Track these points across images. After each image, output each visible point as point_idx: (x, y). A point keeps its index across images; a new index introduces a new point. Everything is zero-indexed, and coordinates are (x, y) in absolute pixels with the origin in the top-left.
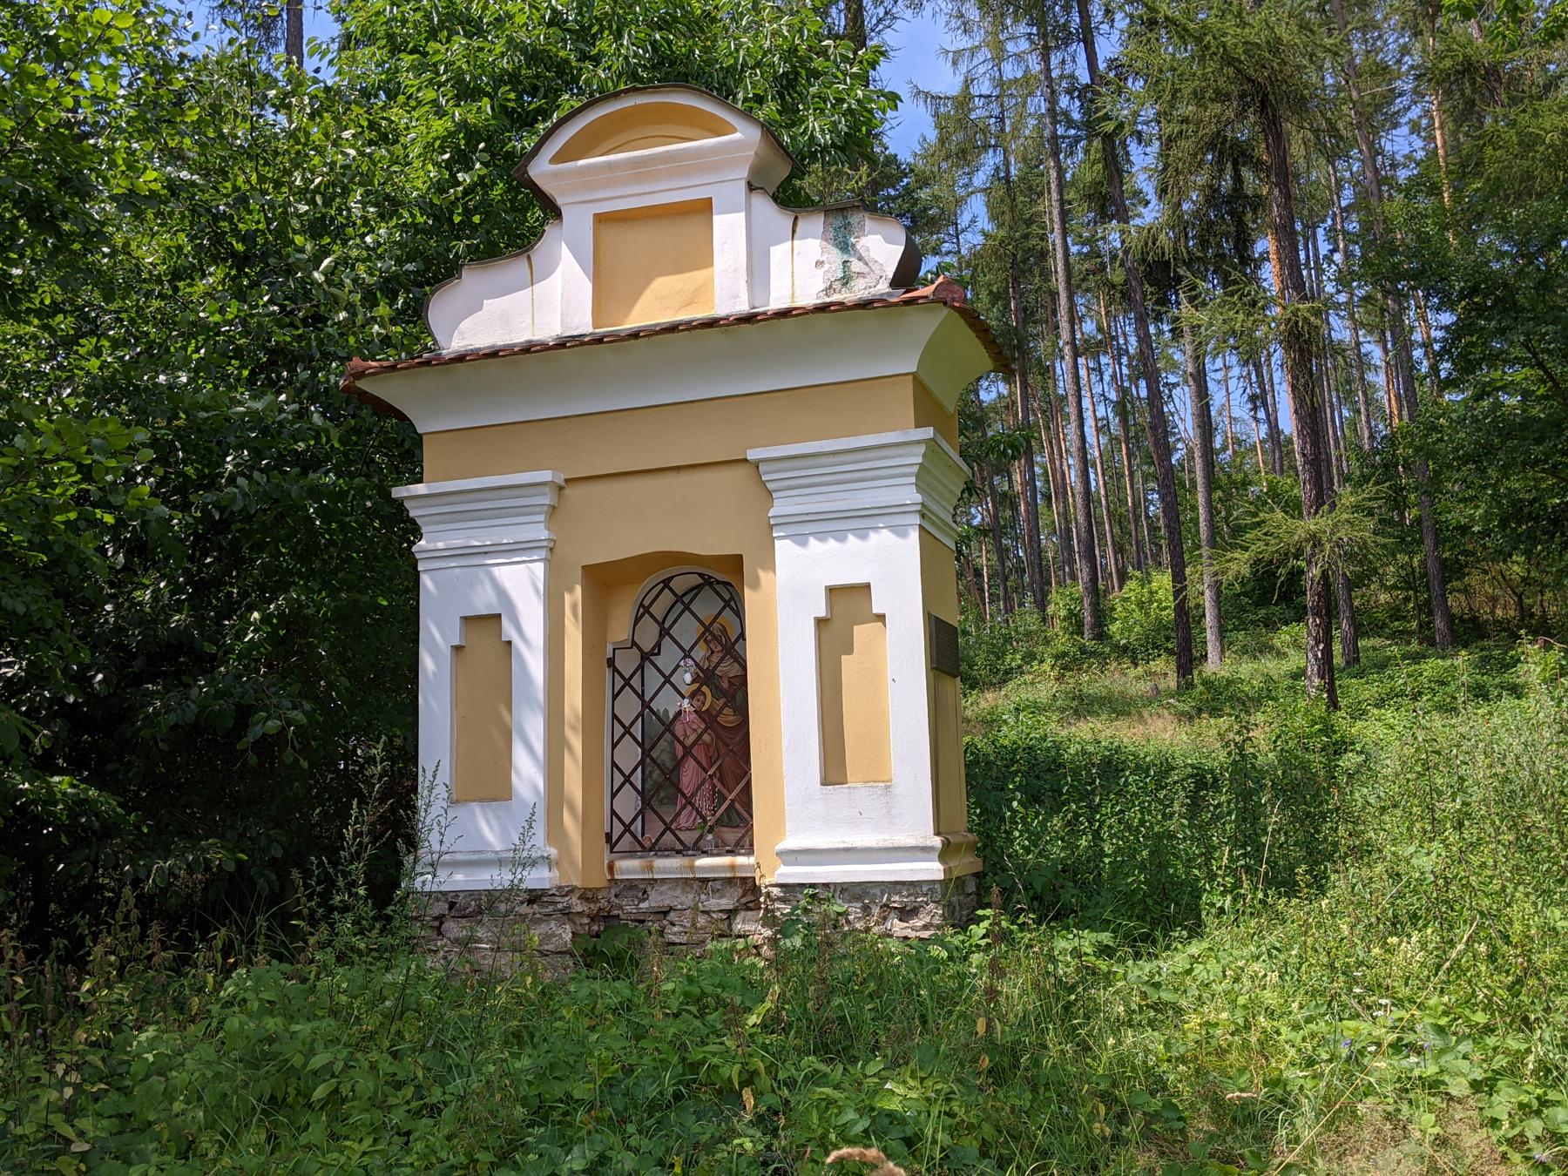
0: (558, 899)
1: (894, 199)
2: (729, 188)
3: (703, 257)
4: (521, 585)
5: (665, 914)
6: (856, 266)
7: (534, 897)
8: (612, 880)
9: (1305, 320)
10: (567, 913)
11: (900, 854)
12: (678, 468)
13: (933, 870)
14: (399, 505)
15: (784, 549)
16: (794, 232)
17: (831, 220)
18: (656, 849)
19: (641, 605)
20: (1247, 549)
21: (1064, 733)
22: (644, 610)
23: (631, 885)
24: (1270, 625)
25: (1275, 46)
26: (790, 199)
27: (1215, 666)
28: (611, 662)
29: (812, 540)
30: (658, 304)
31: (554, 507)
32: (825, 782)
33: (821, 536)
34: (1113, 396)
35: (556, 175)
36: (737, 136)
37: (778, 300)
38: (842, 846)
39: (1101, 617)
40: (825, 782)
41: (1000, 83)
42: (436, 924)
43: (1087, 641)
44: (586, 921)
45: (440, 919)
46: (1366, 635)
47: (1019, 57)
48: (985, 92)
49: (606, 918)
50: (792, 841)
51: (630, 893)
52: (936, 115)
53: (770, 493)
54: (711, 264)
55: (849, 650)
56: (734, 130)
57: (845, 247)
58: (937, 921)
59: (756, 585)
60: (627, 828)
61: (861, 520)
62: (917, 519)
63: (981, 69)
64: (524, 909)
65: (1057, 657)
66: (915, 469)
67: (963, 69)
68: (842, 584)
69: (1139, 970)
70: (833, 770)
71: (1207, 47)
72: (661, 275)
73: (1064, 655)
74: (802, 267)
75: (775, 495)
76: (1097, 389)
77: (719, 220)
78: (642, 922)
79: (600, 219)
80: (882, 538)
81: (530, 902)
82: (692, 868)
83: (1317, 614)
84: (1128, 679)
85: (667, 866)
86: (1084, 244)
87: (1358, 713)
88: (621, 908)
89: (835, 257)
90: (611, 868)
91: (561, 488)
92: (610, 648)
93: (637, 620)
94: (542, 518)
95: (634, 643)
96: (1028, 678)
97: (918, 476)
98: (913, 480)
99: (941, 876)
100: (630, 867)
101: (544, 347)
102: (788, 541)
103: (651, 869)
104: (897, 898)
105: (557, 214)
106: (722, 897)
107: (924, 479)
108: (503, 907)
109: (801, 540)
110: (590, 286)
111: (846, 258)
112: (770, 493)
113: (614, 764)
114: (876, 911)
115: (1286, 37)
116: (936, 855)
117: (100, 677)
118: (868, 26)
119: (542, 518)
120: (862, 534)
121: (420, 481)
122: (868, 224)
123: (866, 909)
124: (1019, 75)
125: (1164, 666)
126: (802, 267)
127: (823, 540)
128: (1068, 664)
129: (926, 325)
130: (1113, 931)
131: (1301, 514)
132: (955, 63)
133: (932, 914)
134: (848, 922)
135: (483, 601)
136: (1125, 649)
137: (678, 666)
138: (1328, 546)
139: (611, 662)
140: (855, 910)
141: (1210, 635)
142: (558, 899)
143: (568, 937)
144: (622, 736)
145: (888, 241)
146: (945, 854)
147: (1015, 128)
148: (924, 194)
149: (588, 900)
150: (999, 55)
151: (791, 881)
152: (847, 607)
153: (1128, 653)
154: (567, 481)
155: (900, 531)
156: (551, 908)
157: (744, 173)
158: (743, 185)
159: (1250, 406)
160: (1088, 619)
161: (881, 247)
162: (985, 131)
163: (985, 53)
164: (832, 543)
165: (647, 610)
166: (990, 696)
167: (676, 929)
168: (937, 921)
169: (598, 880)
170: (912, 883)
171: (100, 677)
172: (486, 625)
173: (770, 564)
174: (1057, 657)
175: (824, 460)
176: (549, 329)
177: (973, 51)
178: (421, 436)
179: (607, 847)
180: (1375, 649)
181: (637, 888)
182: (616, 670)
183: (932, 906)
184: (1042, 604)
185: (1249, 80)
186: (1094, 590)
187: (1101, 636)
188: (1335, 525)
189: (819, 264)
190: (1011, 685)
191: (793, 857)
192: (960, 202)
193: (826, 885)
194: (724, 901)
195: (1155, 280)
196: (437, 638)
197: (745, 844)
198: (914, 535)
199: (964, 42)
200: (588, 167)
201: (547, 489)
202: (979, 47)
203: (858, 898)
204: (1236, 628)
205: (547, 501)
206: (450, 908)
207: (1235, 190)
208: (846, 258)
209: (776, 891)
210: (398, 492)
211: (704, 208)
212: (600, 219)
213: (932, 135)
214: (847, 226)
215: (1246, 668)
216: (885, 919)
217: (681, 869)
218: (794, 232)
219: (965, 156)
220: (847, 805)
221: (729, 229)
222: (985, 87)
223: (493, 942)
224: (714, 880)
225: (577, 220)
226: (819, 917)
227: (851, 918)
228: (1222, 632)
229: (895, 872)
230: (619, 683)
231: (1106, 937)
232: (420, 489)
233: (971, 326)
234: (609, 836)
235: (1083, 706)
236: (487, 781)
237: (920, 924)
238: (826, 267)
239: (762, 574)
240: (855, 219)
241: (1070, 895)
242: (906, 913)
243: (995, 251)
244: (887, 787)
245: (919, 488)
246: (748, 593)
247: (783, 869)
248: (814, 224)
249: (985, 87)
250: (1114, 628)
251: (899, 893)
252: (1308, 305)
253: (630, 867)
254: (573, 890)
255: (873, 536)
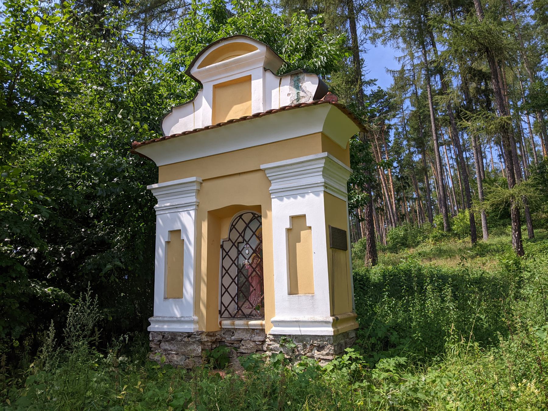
0: (197, 336)
1: (383, 102)
2: (257, 71)
3: (248, 97)
4: (187, 220)
5: (241, 341)
6: (302, 94)
7: (189, 335)
8: (221, 328)
9: (505, 122)
10: (201, 342)
11: (317, 324)
12: (239, 174)
13: (329, 331)
14: (149, 191)
15: (275, 202)
16: (280, 84)
17: (293, 78)
18: (233, 317)
19: (232, 225)
20: (488, 200)
21: (44, 349)
22: (233, 227)
23: (228, 330)
24: (505, 225)
25: (489, 31)
26: (280, 74)
27: (485, 240)
28: (222, 246)
29: (285, 199)
30: (236, 112)
31: (199, 190)
32: (290, 293)
33: (288, 197)
34: (454, 157)
35: (199, 72)
36: (258, 51)
37: (275, 106)
38: (295, 320)
39: (449, 225)
40: (290, 293)
41: (413, 65)
42: (158, 343)
43: (445, 233)
44: (209, 344)
45: (160, 341)
46: (536, 228)
47: (419, 57)
48: (409, 68)
49: (220, 342)
50: (277, 318)
51: (228, 333)
52: (394, 76)
53: (270, 181)
54: (250, 99)
55: (299, 241)
56: (257, 49)
57: (298, 87)
58: (332, 352)
59: (266, 217)
60: (226, 309)
61: (302, 190)
62: (322, 189)
63: (407, 62)
64: (186, 339)
65: (433, 237)
66: (322, 169)
67: (401, 62)
68: (297, 215)
69: (410, 380)
70: (293, 290)
71: (465, 33)
72: (235, 105)
73: (436, 236)
74: (283, 95)
75: (272, 182)
76: (449, 155)
77: (254, 83)
78: (233, 344)
79: (215, 87)
80: (310, 197)
81: (189, 337)
82: (248, 325)
83: (515, 222)
84: (459, 243)
85: (240, 323)
86: (443, 112)
87: (532, 255)
88: (225, 338)
89: (295, 91)
90: (220, 323)
91: (201, 183)
92: (222, 241)
93: (231, 230)
94: (194, 194)
95: (230, 239)
96: (425, 244)
97: (323, 172)
98: (321, 173)
99: (332, 334)
100: (227, 323)
101: (190, 132)
102: (276, 199)
103: (234, 324)
104: (315, 342)
105: (202, 88)
106: (259, 336)
107: (325, 172)
108: (179, 338)
109: (281, 199)
110: (211, 110)
111: (298, 91)
112: (270, 181)
113: (222, 284)
114: (308, 346)
115: (493, 28)
116: (331, 325)
117: (73, 253)
118: (359, 42)
119: (194, 194)
120: (303, 195)
121: (157, 183)
122: (306, 78)
123: (305, 346)
124: (419, 62)
125: (468, 239)
126: (283, 95)
127: (288, 198)
128: (437, 239)
129: (324, 111)
130: (407, 357)
131: (507, 187)
132: (399, 61)
133: (329, 349)
134: (298, 351)
135: (178, 227)
136: (456, 234)
137: (244, 247)
138: (517, 198)
139: (222, 246)
140: (300, 346)
141: (484, 229)
142: (197, 336)
143: (200, 350)
144: (225, 274)
145: (313, 83)
146: (335, 324)
147: (418, 78)
148: (392, 100)
149: (211, 336)
150: (412, 57)
151: (276, 333)
152: (298, 222)
153: (457, 236)
154: (203, 180)
155: (317, 194)
156: (194, 340)
157: (262, 64)
158: (261, 69)
159: (499, 158)
160: (445, 225)
161: (310, 86)
162: (409, 80)
163: (408, 57)
164: (292, 199)
165: (234, 227)
166: (412, 250)
167: (244, 347)
168: (332, 352)
169: (214, 328)
170: (322, 336)
171: (73, 253)
172: (176, 233)
173: (270, 209)
174: (433, 237)
175: (288, 167)
176: (200, 125)
177: (404, 57)
178: (158, 167)
179: (219, 316)
180: (540, 232)
181: (231, 331)
182: (223, 249)
183: (329, 346)
184: (432, 221)
185: (482, 44)
186: (446, 216)
187: (449, 230)
188: (519, 191)
189: (289, 94)
190: (419, 246)
191: (277, 324)
192: (402, 102)
193: (290, 335)
194: (260, 337)
195: (457, 116)
196: (161, 239)
197: (262, 316)
198: (322, 195)
199: (401, 54)
200: (209, 68)
201: (195, 184)
202: (406, 56)
203: (302, 341)
204: (493, 227)
205: (195, 188)
206: (163, 338)
207: (486, 88)
208: (298, 91)
209: (271, 337)
210: (148, 187)
211: (248, 79)
212: (215, 87)
213: (393, 82)
214: (299, 80)
215: (496, 240)
216: (312, 350)
217: (244, 325)
218: (280, 84)
219: (403, 88)
220: (299, 304)
221: (257, 85)
222: (408, 67)
223: (176, 351)
224: (257, 329)
225: (208, 88)
226: (296, 345)
227: (299, 349)
228: (488, 229)
229: (315, 331)
230: (225, 254)
231: (402, 360)
232: (155, 186)
233: (344, 112)
234: (220, 311)
235: (440, 253)
236: (176, 293)
237: (325, 353)
238: (291, 96)
239: (268, 212)
240: (301, 77)
241: (394, 337)
242: (320, 348)
243: (414, 115)
244: (312, 296)
245: (323, 176)
246: (263, 220)
247: (274, 328)
248: (287, 80)
249: (408, 67)
250: (454, 228)
251: (317, 340)
252: (506, 117)
253: (227, 323)
254: (202, 333)
255: (307, 196)
